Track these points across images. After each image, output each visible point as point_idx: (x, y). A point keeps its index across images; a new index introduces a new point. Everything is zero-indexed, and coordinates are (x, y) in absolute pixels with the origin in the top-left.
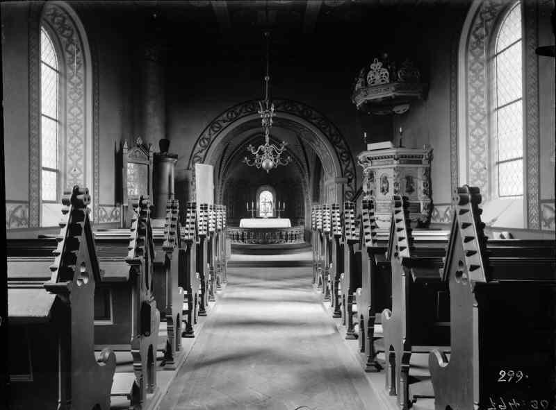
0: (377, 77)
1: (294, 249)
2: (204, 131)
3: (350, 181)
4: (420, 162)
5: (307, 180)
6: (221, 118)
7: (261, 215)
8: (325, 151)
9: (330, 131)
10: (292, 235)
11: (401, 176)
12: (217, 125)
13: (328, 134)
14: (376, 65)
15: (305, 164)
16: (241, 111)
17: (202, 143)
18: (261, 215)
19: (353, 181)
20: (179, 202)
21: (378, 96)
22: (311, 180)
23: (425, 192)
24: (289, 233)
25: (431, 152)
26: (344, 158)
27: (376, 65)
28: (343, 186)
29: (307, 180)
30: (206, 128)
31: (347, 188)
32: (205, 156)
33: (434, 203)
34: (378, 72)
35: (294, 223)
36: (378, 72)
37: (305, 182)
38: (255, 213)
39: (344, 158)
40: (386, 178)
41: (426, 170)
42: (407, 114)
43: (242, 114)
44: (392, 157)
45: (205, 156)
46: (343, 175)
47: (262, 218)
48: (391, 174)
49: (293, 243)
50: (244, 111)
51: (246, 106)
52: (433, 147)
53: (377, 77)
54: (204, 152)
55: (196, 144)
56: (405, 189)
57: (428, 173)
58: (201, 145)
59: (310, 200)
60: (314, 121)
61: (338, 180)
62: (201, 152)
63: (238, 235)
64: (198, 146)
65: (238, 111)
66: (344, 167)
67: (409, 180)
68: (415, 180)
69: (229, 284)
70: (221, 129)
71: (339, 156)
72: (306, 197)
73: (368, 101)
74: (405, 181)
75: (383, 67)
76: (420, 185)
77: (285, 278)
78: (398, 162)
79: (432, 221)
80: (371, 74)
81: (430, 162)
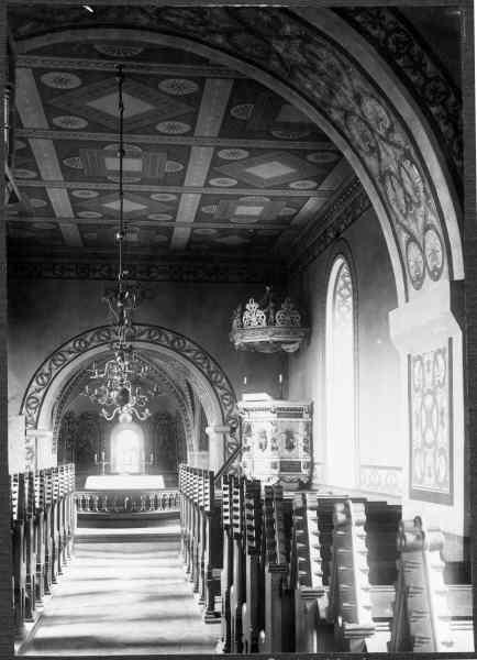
0: (254, 319)
1: (148, 519)
2: (43, 364)
3: (233, 430)
4: (301, 416)
5: (190, 416)
6: (65, 348)
7: (118, 469)
8: (205, 395)
9: (208, 367)
10: (164, 500)
11: (280, 431)
12: (60, 357)
13: (205, 370)
14: (252, 306)
15: (187, 393)
16: (92, 339)
17: (40, 381)
18: (118, 469)
19: (238, 430)
20: (13, 652)
21: (257, 338)
22: (196, 427)
23: (305, 449)
24: (160, 497)
25: (312, 404)
26: (225, 402)
27: (252, 306)
28: (225, 437)
29: (190, 416)
30: (45, 362)
31: (229, 439)
32: (44, 396)
33: (315, 461)
34: (254, 314)
35: (168, 485)
36: (254, 314)
37: (187, 420)
38: (108, 467)
39: (225, 402)
40: (265, 432)
41: (308, 425)
42: (297, 353)
43: (94, 344)
44: (268, 409)
45: (44, 396)
46: (225, 423)
47: (117, 474)
48: (269, 429)
49: (163, 511)
50: (96, 338)
51: (98, 334)
52: (314, 399)
53: (254, 319)
54: (42, 393)
55: (31, 383)
56: (285, 445)
57: (309, 426)
58: (38, 382)
59: (196, 447)
60: (188, 355)
61: (218, 429)
62: (39, 391)
63: (84, 501)
64: (34, 384)
65: (88, 339)
66: (226, 413)
67: (289, 434)
68: (295, 436)
69: (77, 557)
70: (66, 363)
71: (219, 399)
72: (188, 443)
73: (245, 344)
74: (284, 437)
75: (259, 308)
76: (300, 440)
77: (160, 550)
78: (276, 415)
79: (314, 481)
80: (247, 315)
81: (311, 416)
